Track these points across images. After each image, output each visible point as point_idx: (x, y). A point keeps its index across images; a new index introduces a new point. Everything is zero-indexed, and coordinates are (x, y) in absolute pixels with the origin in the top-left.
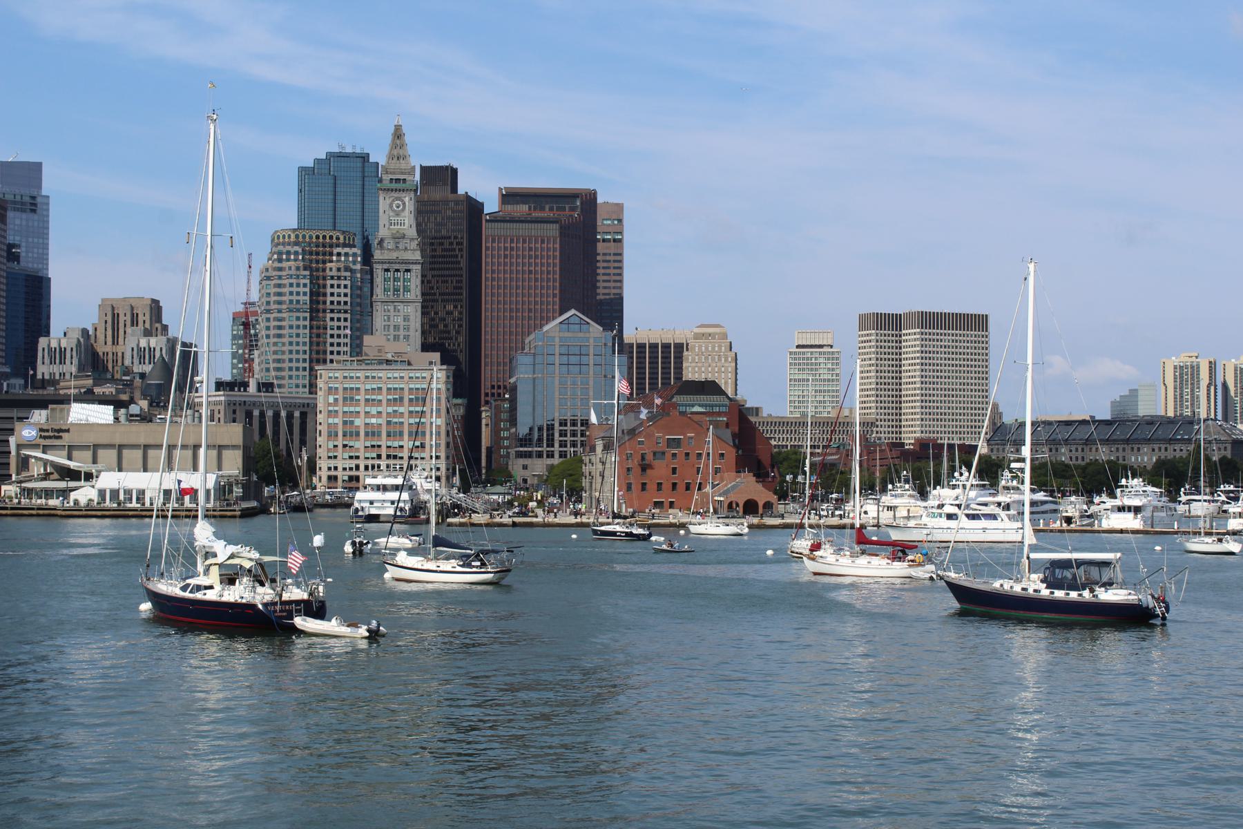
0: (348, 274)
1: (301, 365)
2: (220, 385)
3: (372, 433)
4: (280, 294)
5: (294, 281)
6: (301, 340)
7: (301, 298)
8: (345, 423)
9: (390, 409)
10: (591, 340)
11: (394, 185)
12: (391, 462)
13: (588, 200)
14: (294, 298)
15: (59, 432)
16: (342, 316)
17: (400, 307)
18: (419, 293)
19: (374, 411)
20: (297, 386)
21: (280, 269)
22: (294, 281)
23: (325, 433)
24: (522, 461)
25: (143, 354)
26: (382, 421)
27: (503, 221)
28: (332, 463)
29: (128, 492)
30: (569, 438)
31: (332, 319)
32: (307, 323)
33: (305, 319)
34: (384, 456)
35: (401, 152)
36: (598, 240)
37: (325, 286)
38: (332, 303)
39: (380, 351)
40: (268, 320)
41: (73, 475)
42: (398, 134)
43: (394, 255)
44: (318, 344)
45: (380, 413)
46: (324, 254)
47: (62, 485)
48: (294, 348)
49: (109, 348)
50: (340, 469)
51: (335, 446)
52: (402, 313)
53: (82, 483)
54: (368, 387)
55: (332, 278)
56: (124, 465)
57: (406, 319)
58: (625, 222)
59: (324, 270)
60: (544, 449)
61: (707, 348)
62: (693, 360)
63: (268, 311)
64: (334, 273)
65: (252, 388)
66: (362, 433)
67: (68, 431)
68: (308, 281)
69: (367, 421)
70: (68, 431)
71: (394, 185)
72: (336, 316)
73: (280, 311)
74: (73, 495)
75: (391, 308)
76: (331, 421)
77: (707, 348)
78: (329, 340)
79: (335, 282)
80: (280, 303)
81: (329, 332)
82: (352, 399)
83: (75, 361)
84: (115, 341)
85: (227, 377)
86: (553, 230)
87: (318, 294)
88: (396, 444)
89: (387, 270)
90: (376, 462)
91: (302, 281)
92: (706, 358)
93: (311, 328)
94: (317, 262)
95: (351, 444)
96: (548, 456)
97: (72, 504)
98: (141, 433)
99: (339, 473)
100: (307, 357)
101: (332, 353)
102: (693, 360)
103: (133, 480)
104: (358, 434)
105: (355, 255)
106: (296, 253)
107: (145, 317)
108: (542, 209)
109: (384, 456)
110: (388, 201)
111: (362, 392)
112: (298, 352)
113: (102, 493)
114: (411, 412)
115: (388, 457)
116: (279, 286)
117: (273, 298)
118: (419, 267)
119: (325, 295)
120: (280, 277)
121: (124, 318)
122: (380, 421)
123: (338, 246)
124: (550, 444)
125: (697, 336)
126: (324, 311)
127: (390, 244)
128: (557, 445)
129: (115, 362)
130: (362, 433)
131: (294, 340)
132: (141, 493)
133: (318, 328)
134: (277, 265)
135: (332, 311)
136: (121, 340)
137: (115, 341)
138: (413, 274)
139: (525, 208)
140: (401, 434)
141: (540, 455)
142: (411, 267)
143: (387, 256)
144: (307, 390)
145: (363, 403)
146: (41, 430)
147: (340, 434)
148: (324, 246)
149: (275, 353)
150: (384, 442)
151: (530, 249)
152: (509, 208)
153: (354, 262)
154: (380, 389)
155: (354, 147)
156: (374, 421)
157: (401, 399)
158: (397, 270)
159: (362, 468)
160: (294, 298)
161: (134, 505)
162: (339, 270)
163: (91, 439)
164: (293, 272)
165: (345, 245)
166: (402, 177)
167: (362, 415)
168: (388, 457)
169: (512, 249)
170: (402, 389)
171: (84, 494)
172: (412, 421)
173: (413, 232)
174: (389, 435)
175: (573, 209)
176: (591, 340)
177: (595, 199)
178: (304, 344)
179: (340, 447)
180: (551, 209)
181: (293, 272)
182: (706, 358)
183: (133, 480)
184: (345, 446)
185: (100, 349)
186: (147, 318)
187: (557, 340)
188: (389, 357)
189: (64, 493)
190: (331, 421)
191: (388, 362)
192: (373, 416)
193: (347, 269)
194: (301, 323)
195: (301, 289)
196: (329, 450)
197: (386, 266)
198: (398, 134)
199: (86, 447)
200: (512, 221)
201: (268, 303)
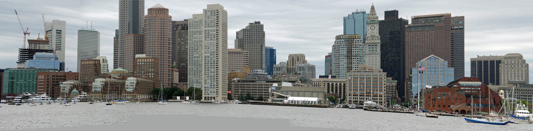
2: (320, 77)
11: (371, 22)
15: (280, 88)
29: (295, 101)
41: (283, 97)
42: (373, 8)
43: (372, 41)
47: (281, 99)
49: (291, 67)
62: (504, 67)
71: (371, 22)
84: (293, 65)
85: (323, 74)
98: (298, 89)
102: (504, 67)
137: (293, 65)
143: (369, 42)
171: (286, 101)
173: (378, 35)
198: (373, 8)
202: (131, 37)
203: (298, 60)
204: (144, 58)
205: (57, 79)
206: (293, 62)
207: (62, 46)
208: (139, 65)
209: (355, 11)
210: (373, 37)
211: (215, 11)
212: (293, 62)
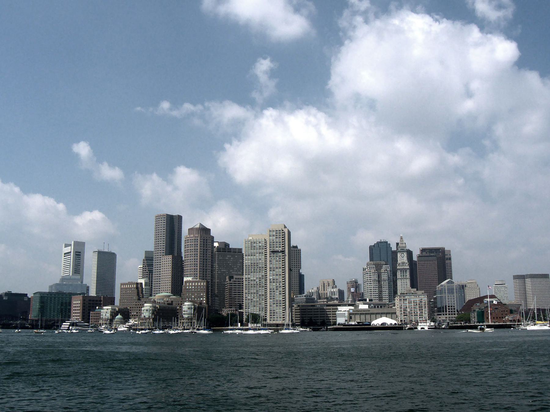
42: (401, 238)
43: (402, 267)
49: (323, 292)
60: (445, 313)
65: (368, 301)
107: (331, 284)
124: (446, 312)
125: (468, 283)
173: (407, 262)
202: (168, 259)
203: (329, 285)
204: (192, 282)
205: (93, 304)
206: (324, 287)
207: (81, 256)
208: (189, 289)
209: (379, 241)
210: (403, 263)
211: (280, 231)
212: (324, 287)
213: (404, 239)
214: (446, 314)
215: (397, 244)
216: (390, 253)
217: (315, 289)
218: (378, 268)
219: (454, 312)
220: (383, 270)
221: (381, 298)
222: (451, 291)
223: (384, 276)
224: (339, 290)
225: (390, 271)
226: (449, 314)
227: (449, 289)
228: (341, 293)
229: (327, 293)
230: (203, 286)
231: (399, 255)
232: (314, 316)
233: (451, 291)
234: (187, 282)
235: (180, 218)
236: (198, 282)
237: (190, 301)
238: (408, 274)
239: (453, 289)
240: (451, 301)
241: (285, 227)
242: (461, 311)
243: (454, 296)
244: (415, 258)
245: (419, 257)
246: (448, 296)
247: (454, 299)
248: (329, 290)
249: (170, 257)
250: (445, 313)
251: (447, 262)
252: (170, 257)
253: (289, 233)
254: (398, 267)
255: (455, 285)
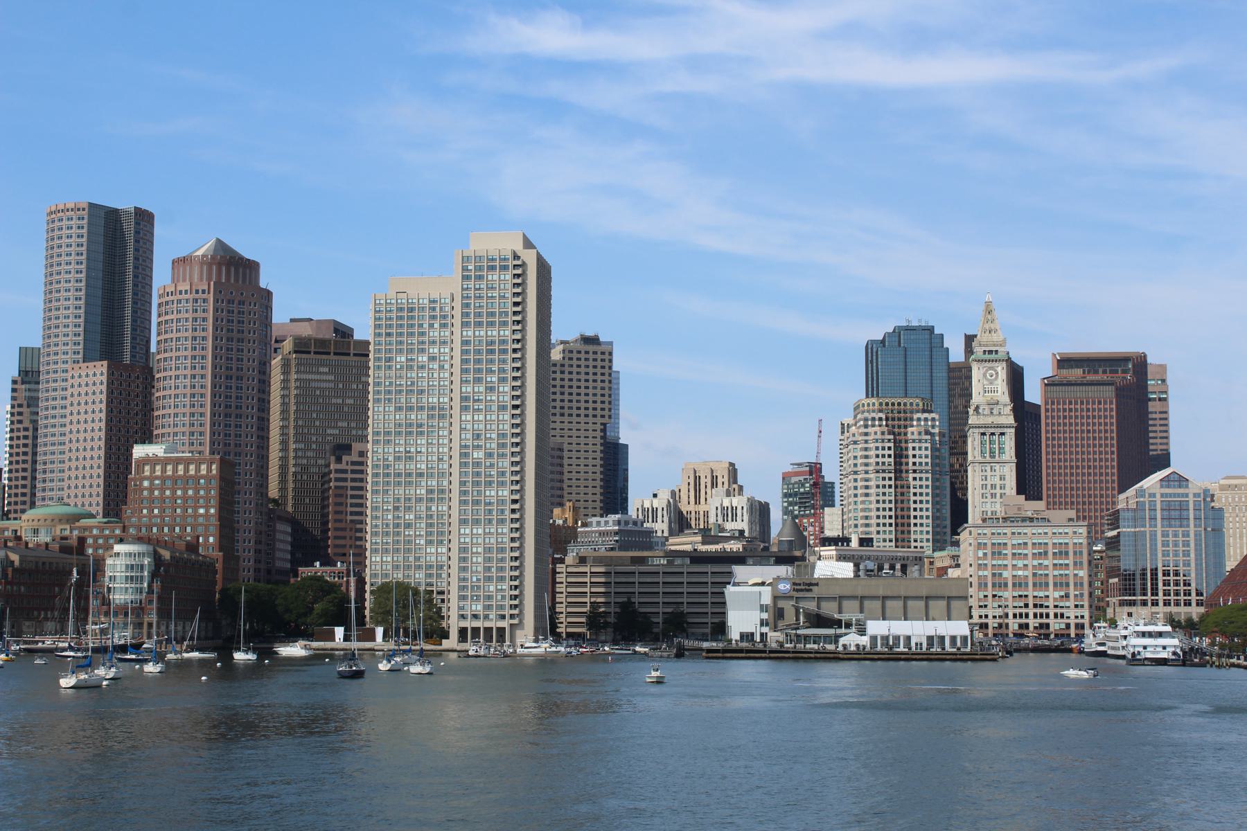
0: (928, 437)
1: (887, 521)
3: (1019, 583)
4: (866, 457)
5: (880, 445)
6: (887, 498)
7: (886, 460)
8: (994, 575)
9: (1035, 563)
10: (1191, 496)
11: (987, 356)
12: (1038, 611)
13: (1139, 364)
14: (880, 460)
16: (924, 476)
17: (997, 467)
18: (1013, 454)
19: (1020, 563)
20: (885, 540)
21: (866, 434)
22: (880, 445)
23: (975, 584)
24: (1127, 609)
25: (729, 513)
26: (1028, 573)
27: (1061, 384)
28: (983, 612)
29: (897, 638)
30: (1172, 588)
31: (915, 479)
32: (892, 483)
33: (890, 479)
34: (1031, 605)
35: (993, 326)
36: (1150, 400)
37: (907, 449)
38: (914, 464)
39: (1019, 509)
40: (856, 480)
43: (989, 420)
44: (902, 502)
45: (1026, 566)
46: (906, 419)
48: (881, 506)
49: (692, 508)
50: (990, 617)
51: (986, 596)
52: (998, 473)
53: (843, 630)
54: (1015, 542)
55: (914, 441)
56: (909, 615)
57: (1002, 478)
58: (1169, 382)
59: (906, 434)
60: (1149, 597)
61: (1233, 499)
63: (856, 473)
64: (916, 437)
65: (854, 543)
66: (1010, 585)
67: (817, 584)
68: (892, 445)
69: (1015, 573)
70: (817, 584)
71: (987, 356)
72: (917, 475)
73: (867, 472)
74: (842, 641)
75: (988, 468)
76: (981, 573)
77: (1233, 499)
78: (913, 498)
79: (917, 445)
80: (866, 465)
81: (912, 490)
82: (1000, 553)
83: (666, 519)
84: (697, 502)
86: (1109, 392)
87: (901, 456)
88: (1041, 594)
89: (983, 434)
90: (1024, 611)
91: (887, 445)
92: (1234, 509)
93: (896, 487)
94: (899, 427)
95: (1000, 594)
96: (1165, 604)
97: (840, 648)
99: (990, 621)
100: (892, 513)
101: (915, 510)
103: (899, 628)
104: (1006, 585)
105: (933, 419)
106: (880, 419)
107: (723, 478)
108: (1096, 372)
109: (1031, 605)
110: (982, 371)
111: (1009, 546)
112: (884, 509)
113: (874, 639)
114: (1055, 565)
115: (1035, 606)
116: (866, 449)
117: (860, 461)
118: (1013, 430)
119: (907, 457)
120: (866, 442)
121: (705, 480)
122: (1026, 573)
123: (918, 412)
124: (1155, 592)
125: (1223, 488)
126: (907, 471)
127: (985, 410)
128: (1161, 593)
129: (698, 519)
130: (1010, 585)
131: (881, 498)
132: (908, 638)
133: (902, 487)
134: (863, 430)
135: (915, 471)
136: (703, 500)
137: (697, 502)
138: (1007, 436)
139: (1079, 372)
140: (1047, 584)
141: (1144, 603)
142: (1005, 430)
143: (981, 420)
144: (893, 544)
145: (1010, 556)
146: (794, 584)
147: (990, 585)
148: (905, 412)
149: (863, 510)
150: (1030, 593)
151: (1088, 410)
152: (1064, 372)
153: (933, 427)
154: (1025, 544)
155: (920, 321)
156: (1020, 573)
157: (1046, 553)
158: (993, 434)
159: (1052, 616)
160: (880, 460)
161: (902, 649)
162: (920, 433)
163: (837, 591)
164: (879, 436)
165: (924, 411)
166: (994, 349)
167: (1010, 567)
168: (1035, 606)
169: (1070, 410)
170: (1066, 544)
171: (852, 640)
172: (1056, 573)
174: (1034, 585)
175: (1125, 372)
176: (1191, 496)
177: (1146, 361)
178: (890, 502)
179: (990, 597)
180: (1104, 372)
181: (879, 436)
182: (1234, 509)
183: (899, 628)
184: (994, 596)
185: (684, 508)
186: (726, 480)
187: (1158, 496)
188: (1029, 514)
189: (837, 638)
190: (981, 573)
191: (1031, 519)
192: (1020, 569)
193: (927, 433)
194: (887, 483)
195: (887, 452)
196: (980, 600)
197: (982, 430)
199: (854, 597)
200: (1069, 384)
201: (855, 465)
202: (94, 378)
203: (714, 484)
204: (165, 462)
213: (996, 314)
214: (1155, 603)
215: (969, 339)
216: (941, 375)
217: (664, 496)
218: (896, 424)
219: (1187, 593)
220: (913, 431)
221: (902, 538)
222: (1175, 513)
223: (920, 453)
224: (751, 502)
225: (941, 434)
226: (1167, 603)
227: (1167, 508)
228: (761, 512)
229: (706, 514)
230: (208, 478)
231: (977, 372)
232: (655, 608)
233: (1175, 513)
234: (146, 461)
235: (144, 218)
236: (187, 462)
237: (139, 540)
238: (1009, 443)
239: (1183, 507)
240: (1167, 548)
241: (528, 244)
242: (1219, 591)
243: (1186, 534)
244: (1033, 393)
245: (1049, 384)
246: (1165, 535)
247: (1186, 544)
248: (716, 500)
249: (100, 370)
250: (1149, 597)
251: (1152, 407)
252: (100, 370)
253: (544, 270)
254: (972, 420)
255: (1192, 490)
